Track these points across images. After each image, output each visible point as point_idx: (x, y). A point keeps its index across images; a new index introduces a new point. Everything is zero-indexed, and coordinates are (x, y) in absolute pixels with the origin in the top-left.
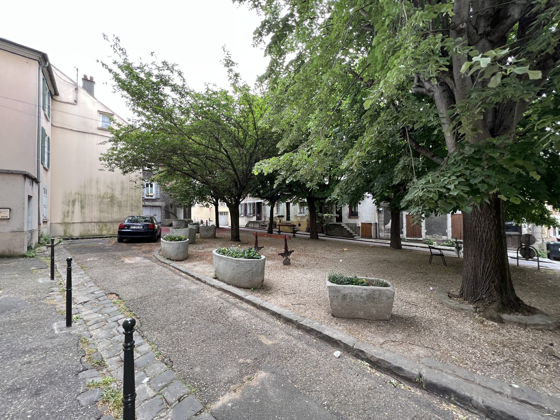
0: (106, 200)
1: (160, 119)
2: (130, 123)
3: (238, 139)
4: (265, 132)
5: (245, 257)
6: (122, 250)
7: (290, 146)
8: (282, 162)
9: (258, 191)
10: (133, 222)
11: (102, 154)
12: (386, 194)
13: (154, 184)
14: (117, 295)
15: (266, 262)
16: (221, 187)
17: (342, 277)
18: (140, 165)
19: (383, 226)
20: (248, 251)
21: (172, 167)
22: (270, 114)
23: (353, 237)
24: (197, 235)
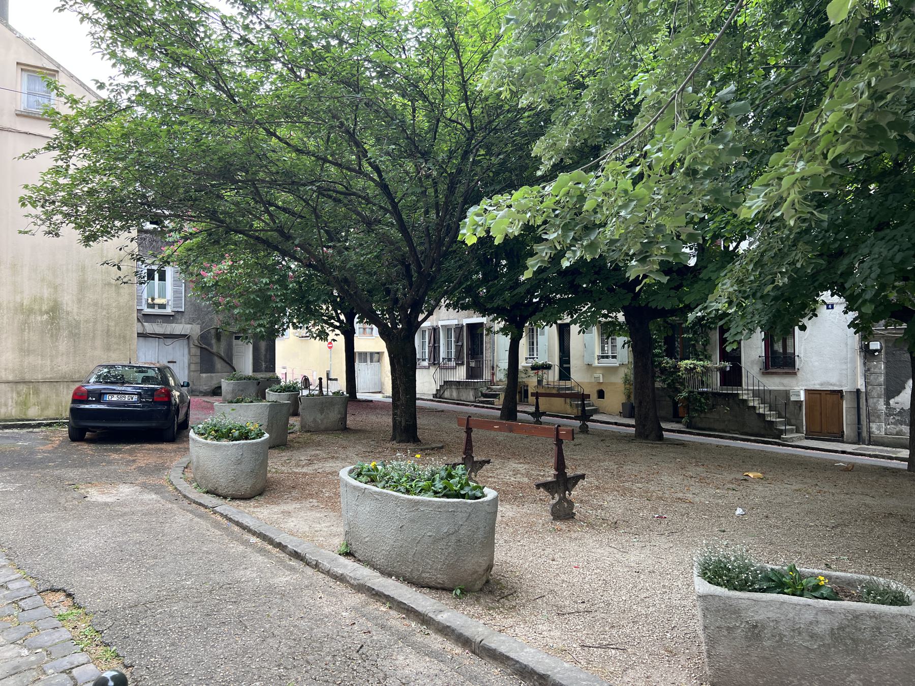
0: (39, 318)
1: (186, 80)
2: (104, 94)
3: (414, 131)
4: (496, 108)
5: (436, 493)
6: (81, 464)
7: (572, 149)
8: (549, 202)
9: (471, 291)
10: (112, 383)
11: (26, 187)
12: (893, 296)
13: (169, 271)
14: (69, 595)
15: (500, 508)
16: (361, 277)
17: (747, 568)
18: (131, 216)
19: (882, 401)
20: (444, 474)
21: (222, 222)
22: (510, 50)
23: (778, 434)
24: (292, 420)
